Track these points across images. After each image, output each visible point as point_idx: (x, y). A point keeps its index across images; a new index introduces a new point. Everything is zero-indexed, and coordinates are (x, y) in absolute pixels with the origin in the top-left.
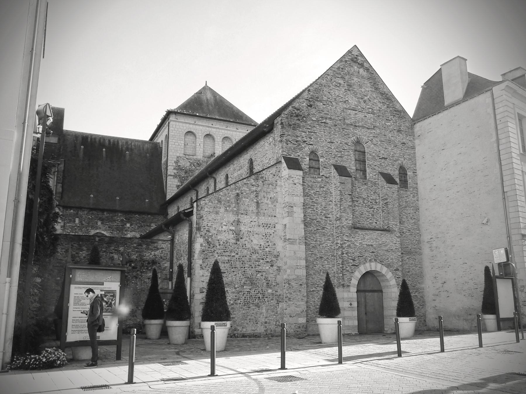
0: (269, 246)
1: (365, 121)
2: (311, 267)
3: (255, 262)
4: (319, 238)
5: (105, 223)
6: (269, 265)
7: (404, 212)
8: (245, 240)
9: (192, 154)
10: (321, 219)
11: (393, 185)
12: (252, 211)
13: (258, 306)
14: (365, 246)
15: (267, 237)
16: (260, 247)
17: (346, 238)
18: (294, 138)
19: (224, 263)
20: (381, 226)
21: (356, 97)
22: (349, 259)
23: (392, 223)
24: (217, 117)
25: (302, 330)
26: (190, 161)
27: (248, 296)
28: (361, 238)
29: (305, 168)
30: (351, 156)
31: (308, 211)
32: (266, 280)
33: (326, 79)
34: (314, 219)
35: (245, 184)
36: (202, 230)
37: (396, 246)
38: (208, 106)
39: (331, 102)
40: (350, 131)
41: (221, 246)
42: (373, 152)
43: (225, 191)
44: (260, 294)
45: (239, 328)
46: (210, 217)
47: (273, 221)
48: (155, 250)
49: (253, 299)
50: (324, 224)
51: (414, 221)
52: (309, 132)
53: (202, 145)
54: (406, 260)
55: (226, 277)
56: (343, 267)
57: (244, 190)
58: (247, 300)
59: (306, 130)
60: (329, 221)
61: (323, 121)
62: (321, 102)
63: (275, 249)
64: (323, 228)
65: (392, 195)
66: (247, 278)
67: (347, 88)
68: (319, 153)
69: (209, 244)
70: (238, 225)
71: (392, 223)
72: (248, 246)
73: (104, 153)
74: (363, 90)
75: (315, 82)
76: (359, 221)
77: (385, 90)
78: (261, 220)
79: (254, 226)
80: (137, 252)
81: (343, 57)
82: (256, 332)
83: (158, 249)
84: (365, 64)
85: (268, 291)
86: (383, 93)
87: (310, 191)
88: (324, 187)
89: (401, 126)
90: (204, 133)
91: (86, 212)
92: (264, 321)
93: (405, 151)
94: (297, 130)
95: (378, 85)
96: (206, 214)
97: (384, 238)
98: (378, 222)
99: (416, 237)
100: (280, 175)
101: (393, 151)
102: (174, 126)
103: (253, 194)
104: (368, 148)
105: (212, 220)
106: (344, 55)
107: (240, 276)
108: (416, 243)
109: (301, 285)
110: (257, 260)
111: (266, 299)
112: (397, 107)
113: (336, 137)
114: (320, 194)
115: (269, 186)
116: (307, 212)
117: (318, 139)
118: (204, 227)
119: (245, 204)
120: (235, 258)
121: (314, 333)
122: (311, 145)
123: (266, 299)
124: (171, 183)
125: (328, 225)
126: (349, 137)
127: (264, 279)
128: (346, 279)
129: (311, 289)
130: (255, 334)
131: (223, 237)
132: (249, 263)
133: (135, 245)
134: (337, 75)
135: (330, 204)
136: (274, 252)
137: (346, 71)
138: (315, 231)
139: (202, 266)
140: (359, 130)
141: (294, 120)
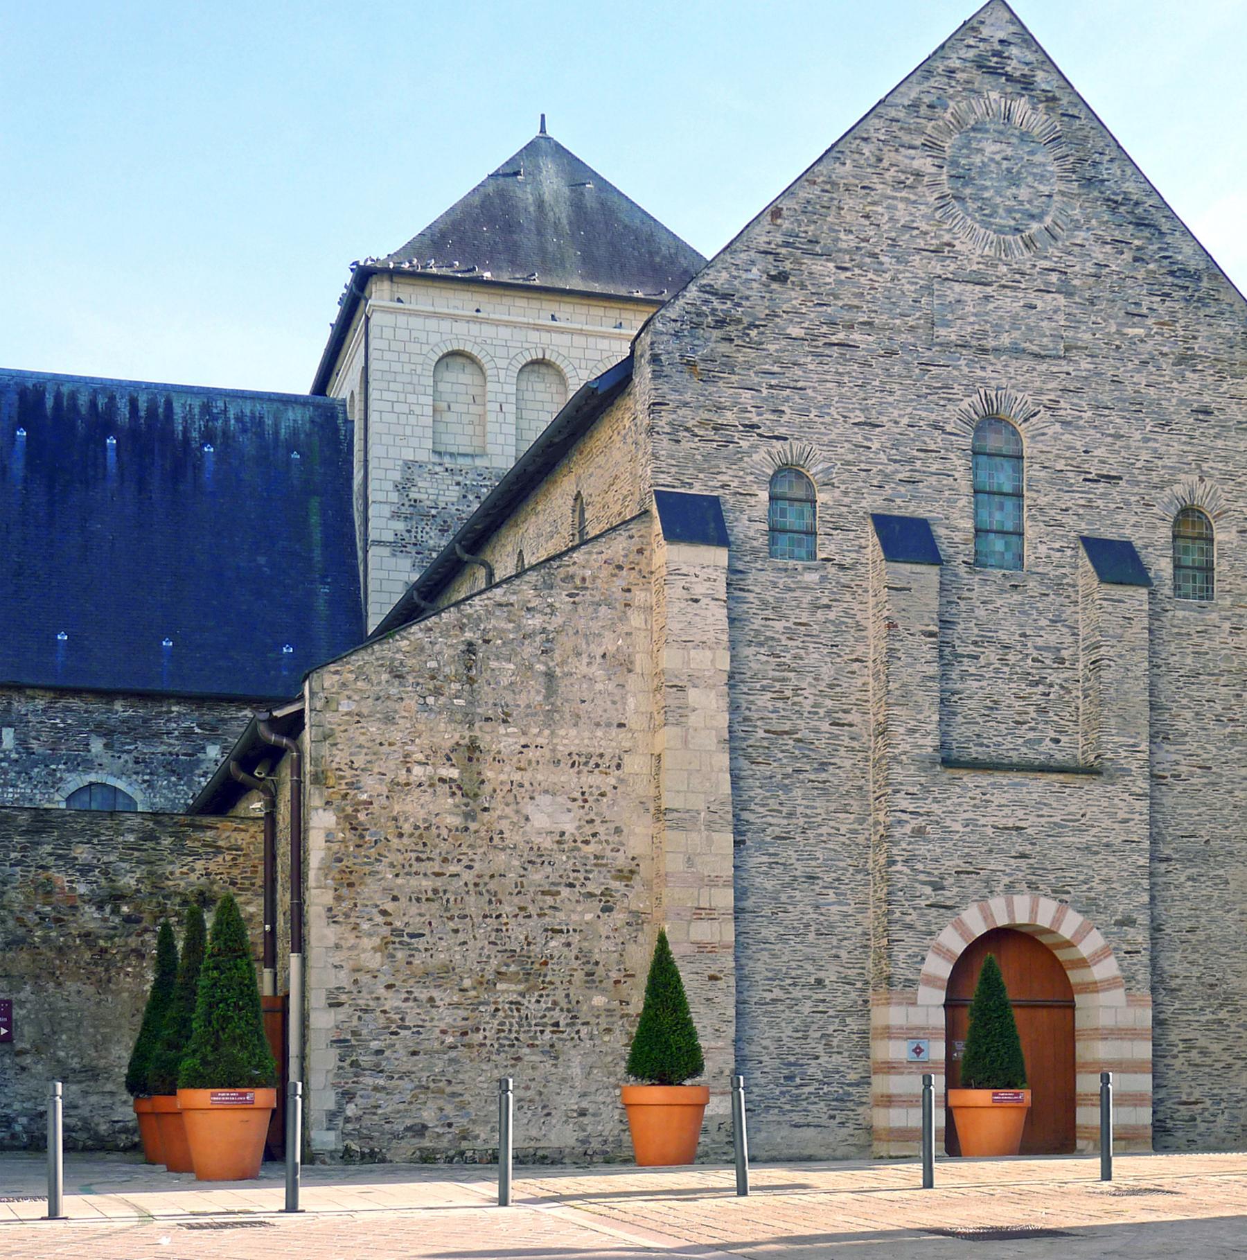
0: (594, 835)
1: (1027, 325)
2: (767, 911)
3: (539, 897)
4: (804, 802)
5: (117, 746)
6: (597, 905)
7: (1186, 695)
8: (500, 818)
9: (469, 450)
10: (816, 731)
11: (1129, 591)
12: (528, 706)
13: (552, 1052)
14: (989, 831)
15: (587, 805)
16: (559, 842)
17: (905, 804)
18: (706, 415)
19: (418, 900)
20: (1079, 753)
21: (986, 225)
22: (917, 881)
23: (1116, 739)
24: (576, 284)
25: (714, 1141)
26: (460, 479)
27: (513, 1017)
28: (973, 802)
29: (751, 534)
30: (957, 475)
31: (760, 703)
32: (584, 960)
33: (856, 156)
34: (786, 733)
35: (500, 605)
36: (331, 782)
37: (1128, 832)
38: (540, 233)
39: (874, 256)
40: (956, 373)
41: (405, 840)
42: (1058, 456)
43: (420, 635)
44: (562, 1010)
45: (477, 1130)
46: (363, 734)
47: (614, 744)
48: (207, 853)
49: (533, 1028)
50: (825, 752)
51: (1229, 730)
52: (771, 387)
53: (510, 408)
54: (1181, 884)
55: (426, 950)
56: (890, 912)
57: (495, 628)
58: (510, 1031)
59: (757, 380)
60: (847, 739)
61: (834, 339)
62: (827, 260)
63: (622, 849)
64: (823, 766)
65: (1119, 631)
66: (509, 954)
67: (949, 191)
68: (813, 471)
69: (358, 833)
70: (470, 759)
71: (1116, 739)
72: (512, 837)
73: (111, 454)
74: (1024, 193)
75: (807, 177)
76: (978, 736)
77: (1129, 187)
78: (566, 741)
79: (534, 764)
80: (139, 862)
81: (935, 53)
82: (541, 1144)
83: (219, 850)
84: (1040, 76)
85: (591, 1000)
86: (1119, 198)
87: (768, 623)
88: (828, 607)
89: (1195, 338)
90: (519, 357)
91: (41, 704)
92: (575, 1107)
93: (1207, 442)
94: (721, 384)
95: (1095, 164)
96: (347, 722)
97: (1074, 801)
98: (1064, 739)
99: (1236, 793)
100: (643, 566)
101: (1150, 444)
102: (388, 333)
103: (530, 644)
104: (1033, 437)
105: (370, 744)
106: (942, 47)
107: (482, 948)
108: (1232, 819)
109: (713, 978)
110: (547, 888)
111: (584, 1031)
112: (1184, 253)
113: (890, 399)
114: (814, 633)
115: (596, 611)
116: (753, 707)
117: (812, 416)
118: (340, 770)
119: (498, 683)
120: (462, 883)
121: (775, 1153)
122: (777, 438)
123: (584, 1031)
124: (384, 575)
125: (842, 752)
126: (949, 400)
127: (577, 958)
128: (902, 956)
129: (766, 994)
130: (540, 1153)
131: (414, 807)
132: (516, 900)
133: (131, 838)
134: (906, 138)
135: (853, 673)
136: (614, 859)
137: (948, 116)
138: (786, 776)
139: (333, 913)
140: (999, 367)
141: (707, 340)
